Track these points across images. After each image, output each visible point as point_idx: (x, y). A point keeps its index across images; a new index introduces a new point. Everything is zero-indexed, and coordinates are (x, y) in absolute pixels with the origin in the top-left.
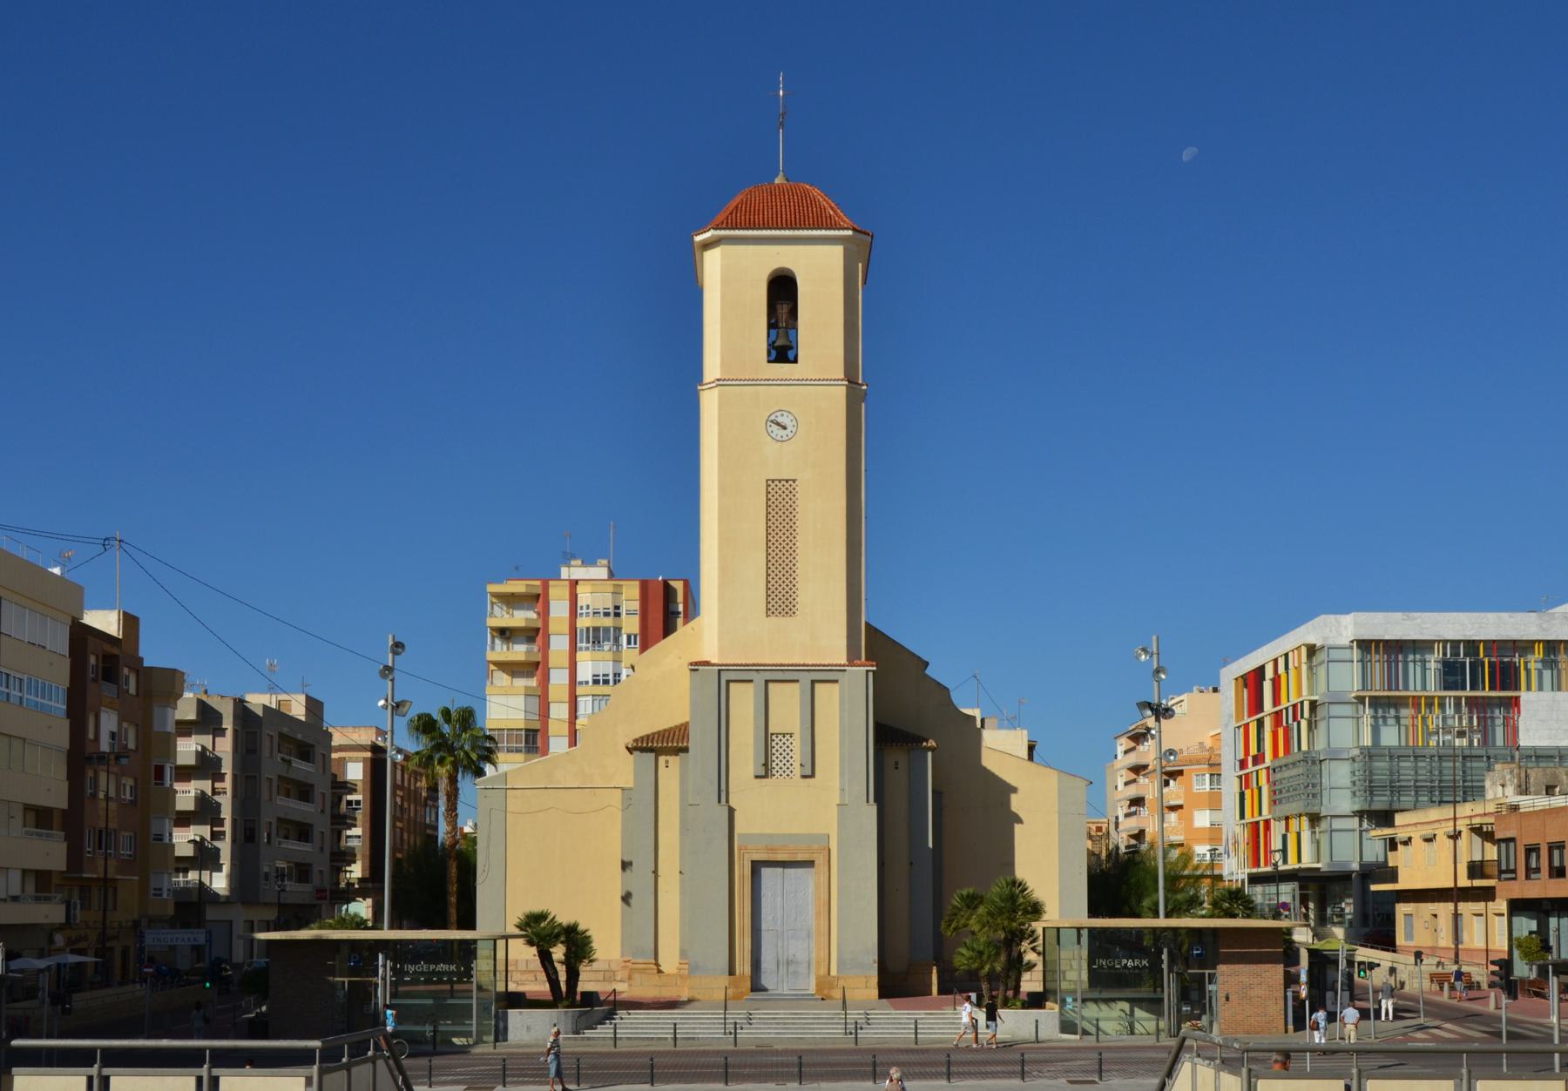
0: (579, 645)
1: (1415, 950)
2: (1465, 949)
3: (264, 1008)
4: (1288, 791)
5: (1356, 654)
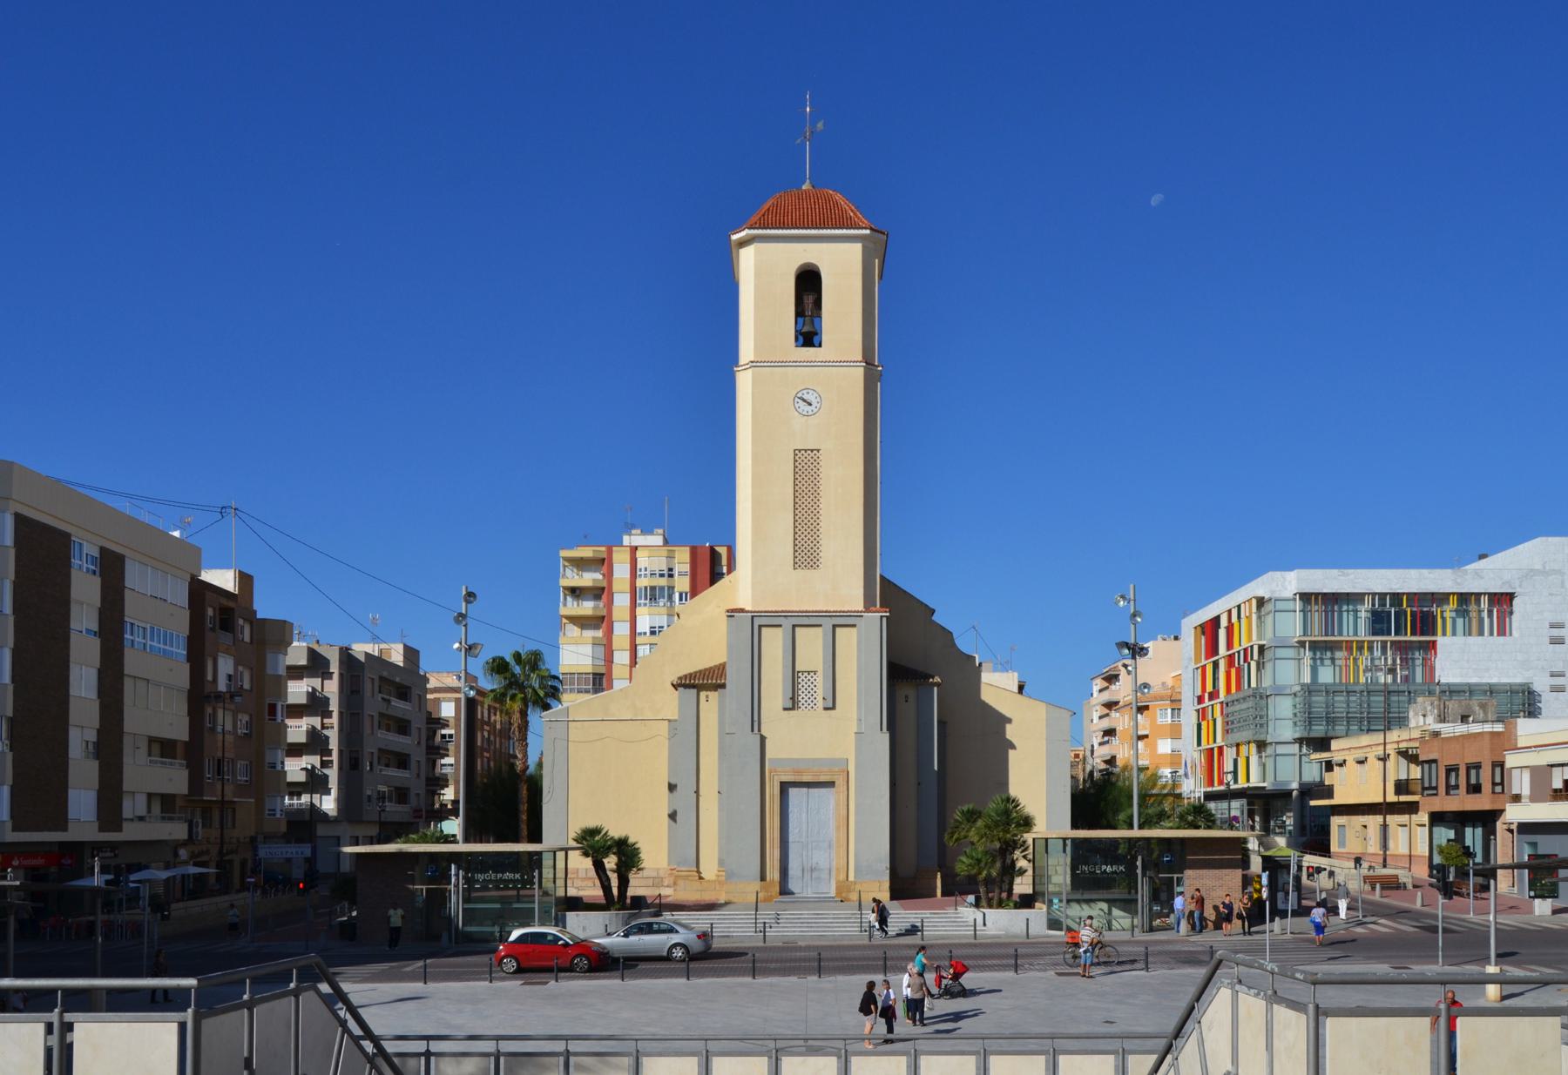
0: (638, 601)
1: (1354, 856)
2: (1391, 855)
3: (354, 914)
4: (1239, 722)
5: (1298, 605)
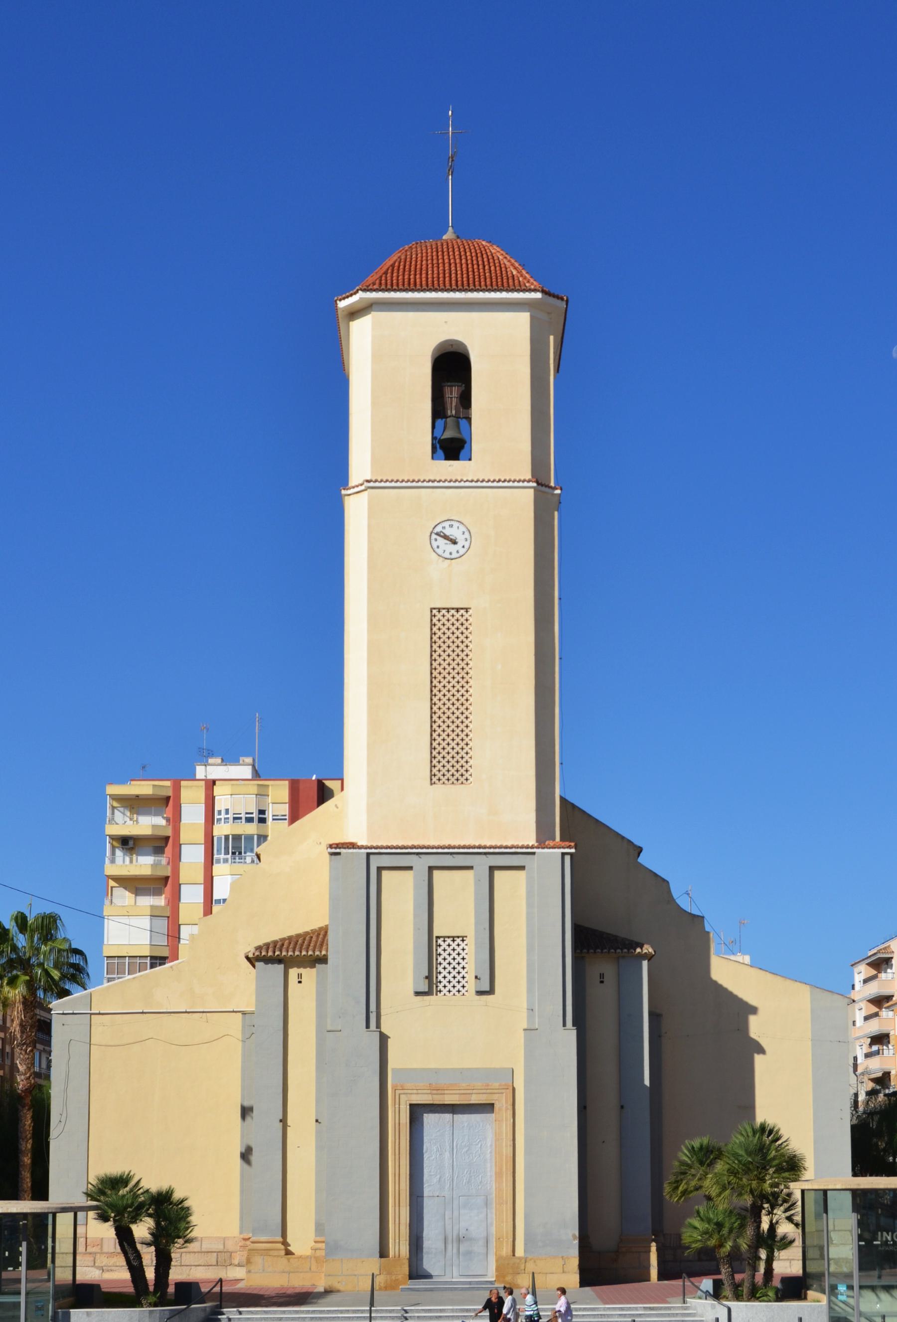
0: (215, 856)
